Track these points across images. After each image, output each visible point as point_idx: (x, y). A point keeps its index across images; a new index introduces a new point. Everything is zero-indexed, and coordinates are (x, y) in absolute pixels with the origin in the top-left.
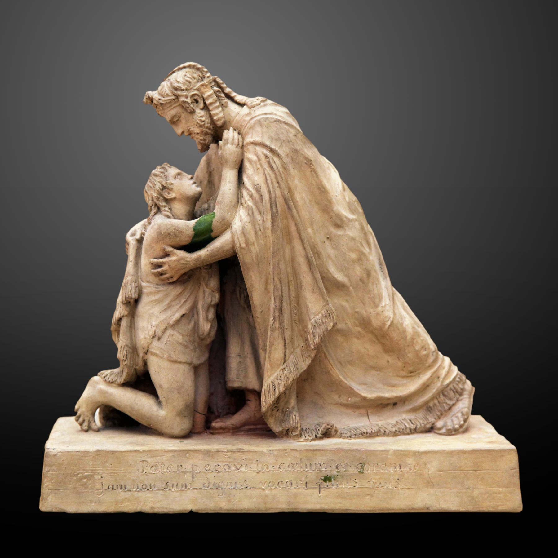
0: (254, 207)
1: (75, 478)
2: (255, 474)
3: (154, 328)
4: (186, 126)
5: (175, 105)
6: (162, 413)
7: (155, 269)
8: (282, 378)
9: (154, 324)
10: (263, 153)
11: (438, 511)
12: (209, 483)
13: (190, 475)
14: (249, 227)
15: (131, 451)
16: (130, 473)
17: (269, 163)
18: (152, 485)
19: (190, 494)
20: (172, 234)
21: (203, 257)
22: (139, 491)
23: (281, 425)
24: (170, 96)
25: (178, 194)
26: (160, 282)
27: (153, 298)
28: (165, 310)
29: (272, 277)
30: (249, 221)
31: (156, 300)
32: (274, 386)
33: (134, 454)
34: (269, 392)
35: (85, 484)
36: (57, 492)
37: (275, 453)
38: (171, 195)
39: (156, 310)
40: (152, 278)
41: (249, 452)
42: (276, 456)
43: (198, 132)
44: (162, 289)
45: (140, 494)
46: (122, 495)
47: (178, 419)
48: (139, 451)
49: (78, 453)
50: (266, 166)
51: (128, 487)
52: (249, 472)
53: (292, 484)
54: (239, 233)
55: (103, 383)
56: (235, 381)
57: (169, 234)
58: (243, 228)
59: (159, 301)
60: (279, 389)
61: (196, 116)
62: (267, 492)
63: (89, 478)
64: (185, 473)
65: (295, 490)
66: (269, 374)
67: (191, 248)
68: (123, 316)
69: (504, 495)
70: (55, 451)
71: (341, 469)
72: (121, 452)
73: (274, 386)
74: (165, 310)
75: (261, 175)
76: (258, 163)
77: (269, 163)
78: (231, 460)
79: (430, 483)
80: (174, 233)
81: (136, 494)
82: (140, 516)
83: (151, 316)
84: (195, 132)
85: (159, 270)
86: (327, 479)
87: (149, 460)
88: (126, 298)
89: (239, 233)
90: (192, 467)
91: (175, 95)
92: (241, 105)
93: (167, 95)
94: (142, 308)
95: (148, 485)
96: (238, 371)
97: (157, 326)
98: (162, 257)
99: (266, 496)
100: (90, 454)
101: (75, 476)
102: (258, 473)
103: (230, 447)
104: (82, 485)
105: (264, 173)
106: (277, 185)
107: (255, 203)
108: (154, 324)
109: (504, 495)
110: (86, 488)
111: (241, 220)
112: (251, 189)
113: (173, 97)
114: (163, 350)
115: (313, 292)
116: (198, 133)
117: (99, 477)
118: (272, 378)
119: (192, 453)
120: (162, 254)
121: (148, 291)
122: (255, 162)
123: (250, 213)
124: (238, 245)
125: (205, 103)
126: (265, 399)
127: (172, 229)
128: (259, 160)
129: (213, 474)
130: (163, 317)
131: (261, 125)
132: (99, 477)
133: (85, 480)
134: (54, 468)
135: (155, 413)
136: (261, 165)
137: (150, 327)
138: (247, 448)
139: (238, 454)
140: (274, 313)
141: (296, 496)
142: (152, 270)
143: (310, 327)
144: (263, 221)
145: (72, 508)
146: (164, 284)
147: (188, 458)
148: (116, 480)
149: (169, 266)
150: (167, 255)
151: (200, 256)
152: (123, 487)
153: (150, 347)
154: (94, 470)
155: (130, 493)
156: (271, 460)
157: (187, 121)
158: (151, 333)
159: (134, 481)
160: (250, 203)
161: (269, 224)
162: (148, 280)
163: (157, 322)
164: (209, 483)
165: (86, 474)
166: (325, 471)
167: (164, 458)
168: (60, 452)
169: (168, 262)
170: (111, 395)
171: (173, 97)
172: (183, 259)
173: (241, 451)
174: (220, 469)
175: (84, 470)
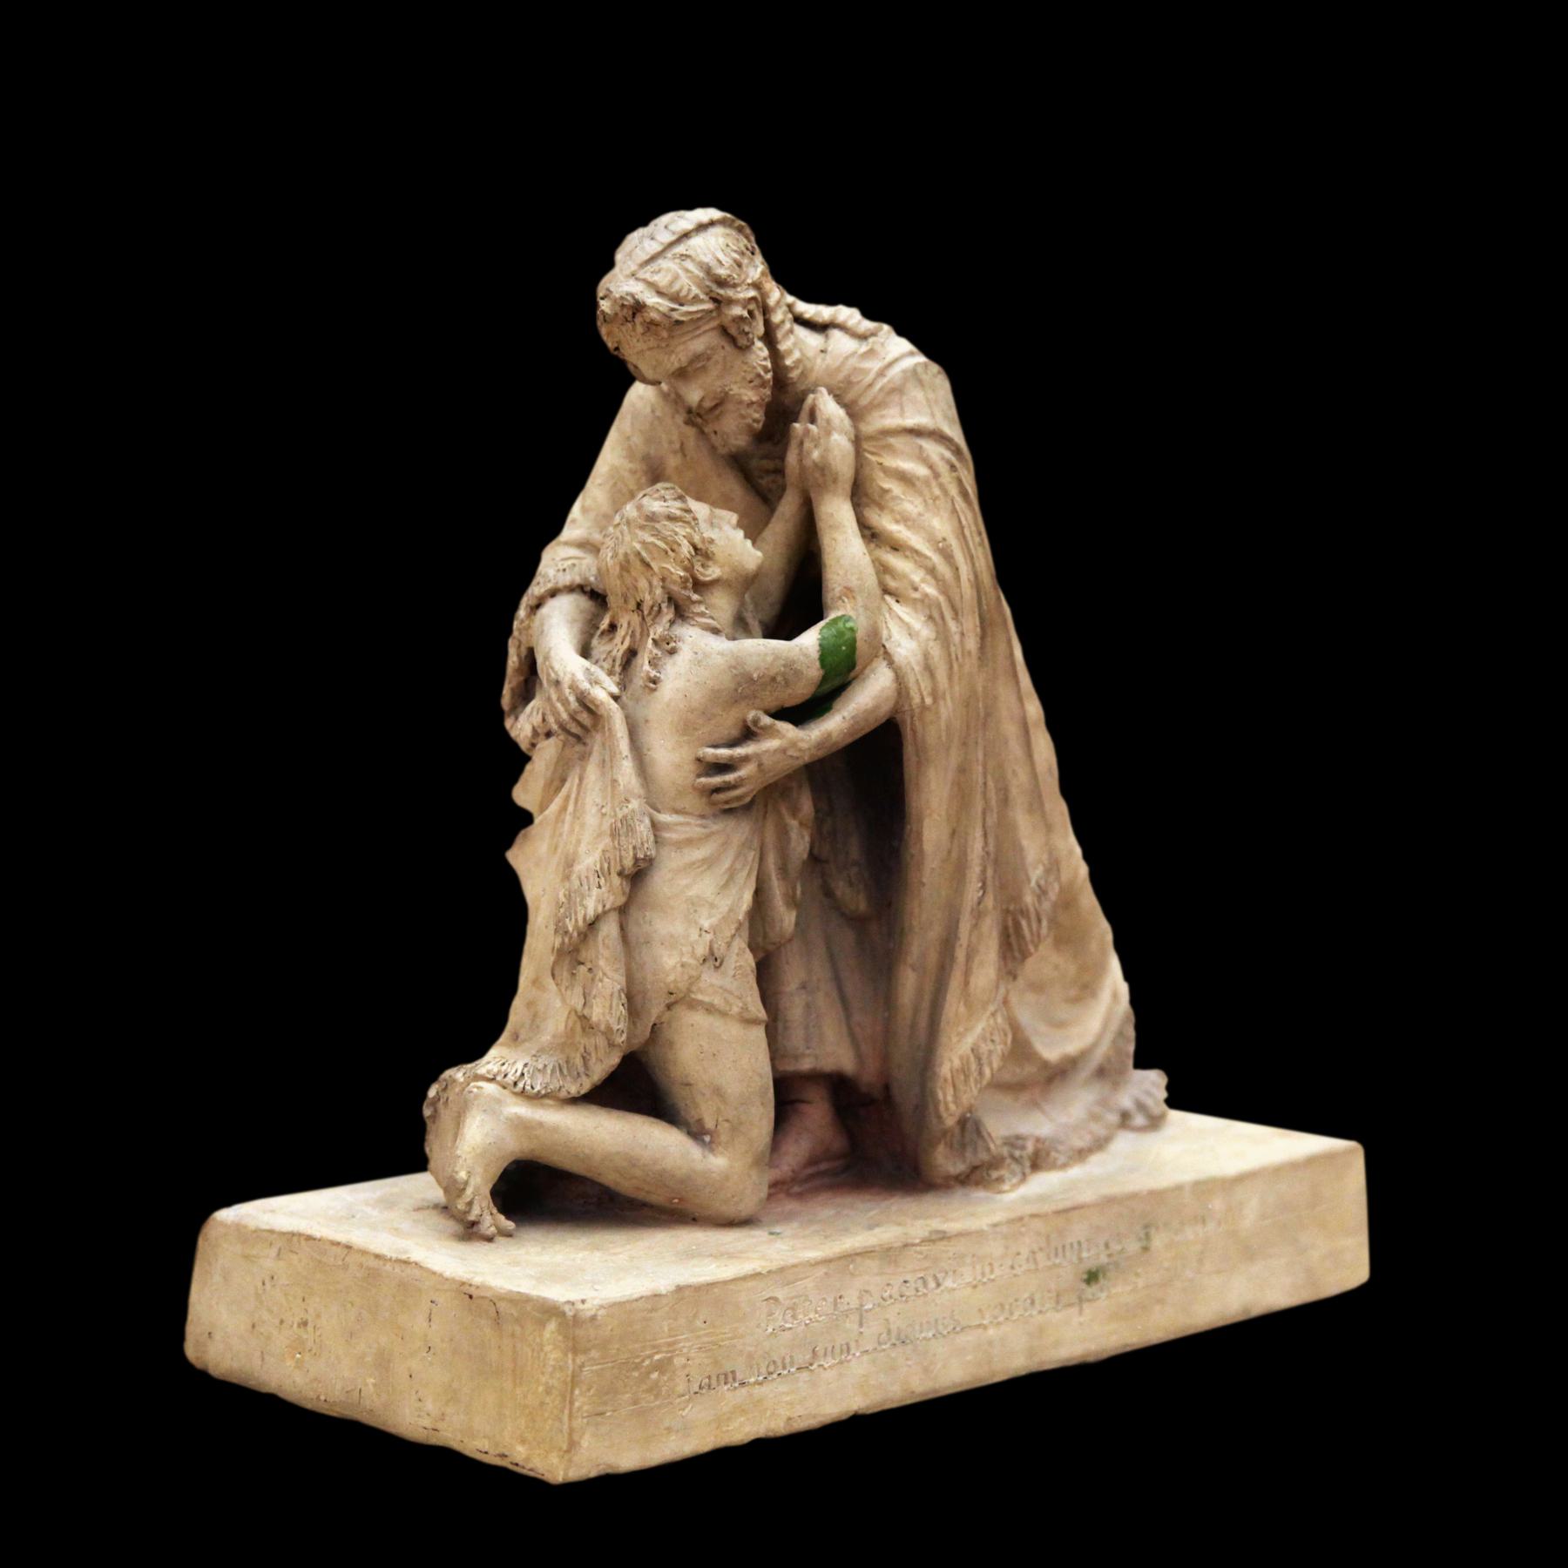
0: (942, 599)
1: (636, 1374)
2: (969, 1290)
3: (708, 937)
4: (718, 383)
5: (707, 327)
6: (718, 1162)
7: (707, 775)
8: (996, 1038)
9: (706, 924)
10: (943, 458)
11: (235, 1381)
12: (889, 1332)
13: (855, 1317)
14: (936, 652)
15: (744, 1278)
16: (742, 1336)
18: (788, 1360)
19: (858, 1367)
20: (779, 679)
21: (834, 735)
22: (760, 1384)
23: (962, 1155)
24: (702, 301)
25: (727, 569)
26: (708, 811)
27: (698, 854)
28: (726, 885)
29: (981, 781)
30: (933, 635)
31: (704, 860)
32: (978, 1059)
33: (751, 1284)
34: (967, 1077)
35: (656, 1383)
36: (599, 1419)
37: (1004, 1229)
38: (709, 572)
39: (706, 886)
40: (693, 802)
41: (960, 1235)
42: (1005, 1237)
43: (754, 399)
44: (715, 828)
45: (765, 1389)
46: (730, 1397)
47: (754, 1174)
48: (759, 1274)
49: (640, 1304)
51: (739, 1376)
52: (959, 1288)
53: (1033, 1302)
54: (917, 668)
55: (513, 1099)
56: (803, 1055)
57: (773, 679)
58: (926, 656)
59: (709, 863)
60: (990, 1064)
61: (753, 357)
62: (991, 1332)
63: (661, 1367)
64: (846, 1314)
65: (1040, 1318)
66: (961, 1029)
67: (801, 714)
68: (605, 913)
69: (1337, 1258)
70: (586, 1306)
71: (1116, 1247)
72: (725, 1283)
73: (978, 1059)
74: (726, 885)
75: (946, 515)
76: (934, 484)
78: (926, 1264)
79: (1249, 1253)
80: (783, 674)
81: (757, 1390)
82: (762, 1448)
83: (695, 903)
84: (745, 398)
85: (717, 780)
86: (1092, 1277)
87: (780, 1294)
88: (636, 860)
89: (917, 668)
90: (860, 1298)
91: (714, 300)
92: (820, 328)
93: (696, 300)
94: (662, 883)
95: (779, 1364)
96: (807, 1028)
97: (715, 930)
98: (732, 744)
99: (990, 1343)
100: (664, 1301)
101: (637, 1367)
102: (975, 1287)
103: (886, 1234)
104: (649, 1390)
105: (954, 511)
107: (944, 590)
108: (706, 924)
109: (1337, 1258)
110: (657, 1397)
111: (912, 634)
112: (929, 553)
113: (709, 306)
114: (731, 993)
115: (1030, 811)
116: (753, 403)
117: (683, 1360)
118: (969, 1040)
119: (859, 1259)
120: (735, 733)
121: (683, 836)
122: (927, 483)
123: (936, 615)
124: (916, 700)
125: (767, 323)
126: (955, 1096)
127: (778, 667)
128: (937, 475)
129: (898, 1307)
130: (724, 904)
132: (683, 1360)
133: (655, 1376)
134: (594, 1354)
135: (699, 1167)
136: (941, 486)
137: (694, 935)
138: (952, 1227)
139: (941, 1246)
140: (984, 871)
141: (1041, 1330)
142: (703, 780)
143: (1029, 899)
144: (962, 634)
145: (629, 1459)
146: (715, 816)
147: (852, 1275)
148: (716, 1362)
149: (760, 765)
150: (748, 733)
151: (829, 735)
152: (728, 1377)
153: (694, 988)
154: (674, 1343)
155: (744, 1391)
156: (995, 1248)
157: (726, 369)
158: (701, 950)
159: (750, 1356)
160: (930, 590)
161: (972, 644)
162: (679, 805)
163: (714, 920)
164: (889, 1332)
165: (657, 1357)
166: (1094, 1257)
167: (809, 1283)
168: (602, 1307)
169: (757, 755)
170: (555, 1129)
171: (709, 306)
172: (794, 744)
173: (943, 1237)
174: (910, 1292)
175: (654, 1347)
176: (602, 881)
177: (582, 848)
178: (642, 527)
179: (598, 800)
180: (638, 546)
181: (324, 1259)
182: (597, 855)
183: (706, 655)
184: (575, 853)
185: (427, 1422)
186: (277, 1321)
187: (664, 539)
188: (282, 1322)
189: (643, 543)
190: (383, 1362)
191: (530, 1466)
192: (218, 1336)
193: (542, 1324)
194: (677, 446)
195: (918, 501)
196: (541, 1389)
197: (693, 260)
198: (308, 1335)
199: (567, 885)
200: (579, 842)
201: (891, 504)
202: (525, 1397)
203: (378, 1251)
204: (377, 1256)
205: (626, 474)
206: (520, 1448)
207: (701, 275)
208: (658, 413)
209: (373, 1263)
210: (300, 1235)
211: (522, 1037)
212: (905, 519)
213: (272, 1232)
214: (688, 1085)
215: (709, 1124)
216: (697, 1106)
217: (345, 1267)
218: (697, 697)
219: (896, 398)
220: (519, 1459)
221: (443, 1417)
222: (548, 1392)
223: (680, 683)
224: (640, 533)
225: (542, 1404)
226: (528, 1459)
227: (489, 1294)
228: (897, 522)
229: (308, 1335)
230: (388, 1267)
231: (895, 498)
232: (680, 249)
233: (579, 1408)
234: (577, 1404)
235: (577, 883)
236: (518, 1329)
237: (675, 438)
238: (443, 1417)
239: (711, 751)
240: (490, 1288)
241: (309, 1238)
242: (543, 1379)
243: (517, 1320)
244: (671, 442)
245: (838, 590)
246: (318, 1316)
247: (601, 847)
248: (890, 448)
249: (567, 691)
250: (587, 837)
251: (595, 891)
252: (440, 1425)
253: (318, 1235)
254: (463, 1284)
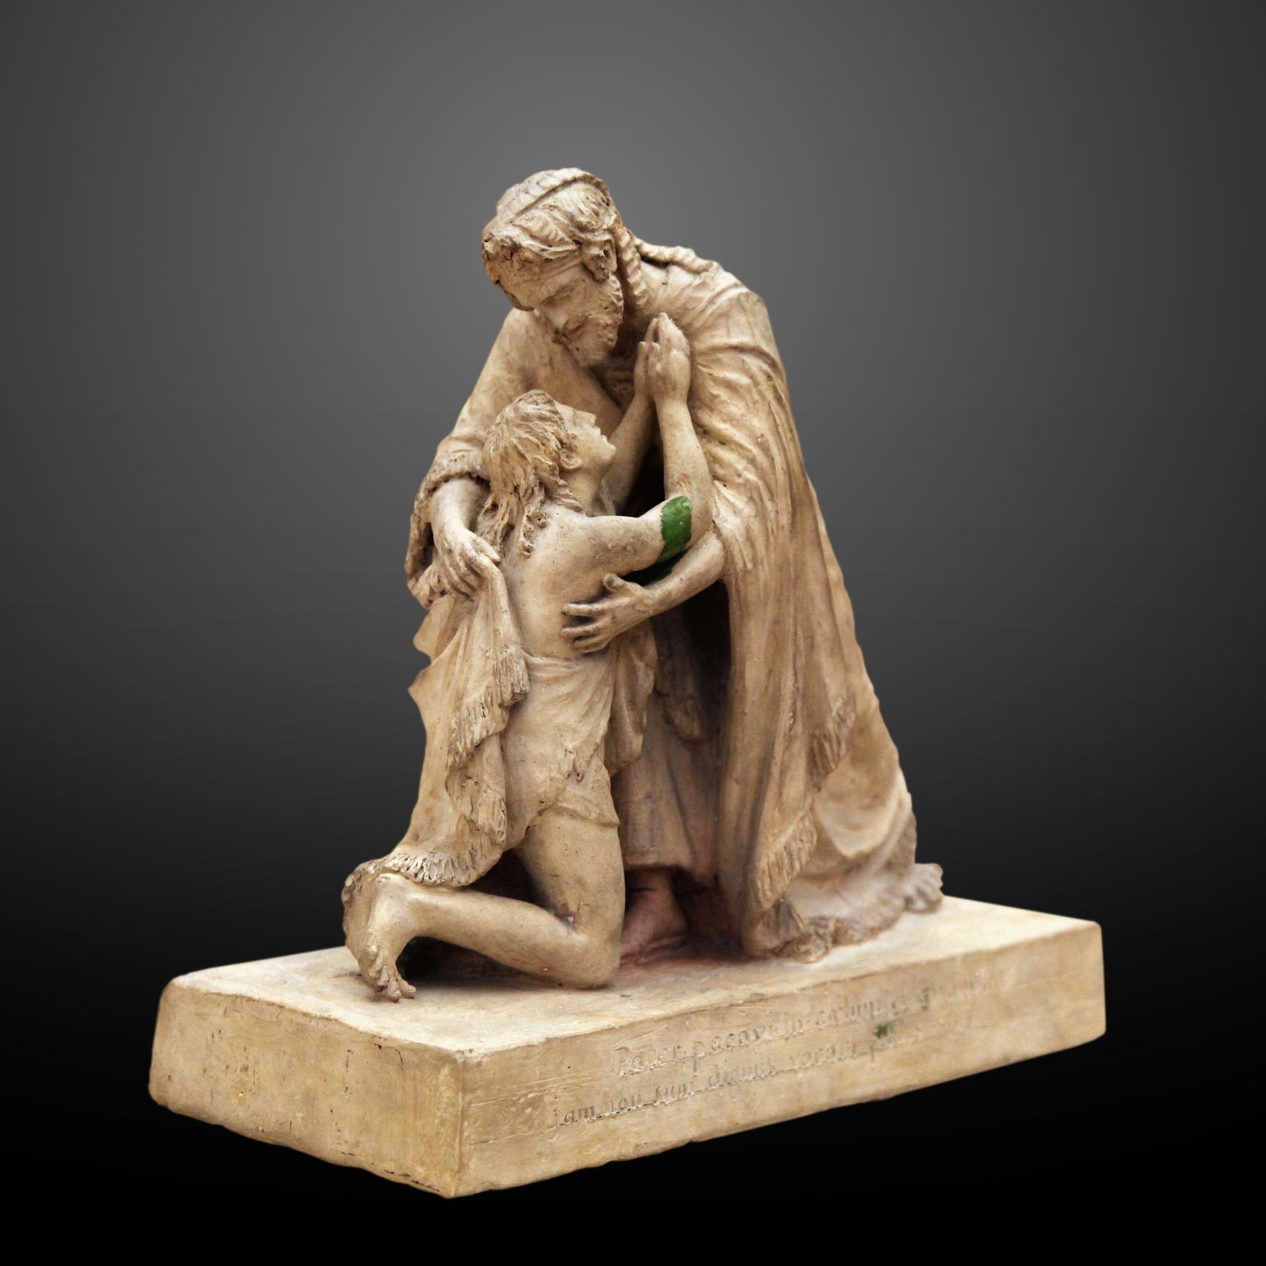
0: (760, 483)
1: (513, 1109)
2: (783, 1041)
3: (572, 757)
4: (580, 309)
5: (571, 264)
6: (580, 938)
7: (571, 625)
8: (804, 838)
9: (570, 746)
10: (761, 370)
12: (718, 1075)
13: (690, 1064)
14: (756, 526)
15: (601, 1032)
16: (599, 1079)
18: (636, 1098)
19: (693, 1104)
20: (629, 548)
21: (674, 594)
22: (614, 1117)
23: (777, 933)
24: (567, 243)
25: (587, 459)
26: (572, 654)
27: (564, 689)
28: (586, 715)
29: (792, 630)
30: (753, 513)
31: (568, 695)
32: (790, 855)
33: (606, 1037)
34: (781, 869)
35: (530, 1117)
36: (484, 1146)
37: (811, 992)
38: (573, 461)
39: (570, 716)
40: (559, 648)
41: (775, 997)
42: (812, 999)
43: (609, 322)
44: (577, 668)
45: (617, 1122)
46: (589, 1128)
47: (609, 948)
48: (613, 1029)
49: (517, 1053)
51: (597, 1111)
52: (774, 1040)
53: (834, 1052)
54: (740, 540)
55: (415, 887)
56: (648, 852)
57: (624, 548)
58: (748, 530)
59: (572, 697)
60: (800, 859)
61: (608, 288)
62: (800, 1075)
63: (534, 1104)
64: (683, 1061)
65: (840, 1064)
66: (776, 831)
67: (647, 576)
68: (488, 737)
69: (1079, 1016)
70: (473, 1054)
71: (901, 1007)
72: (586, 1036)
73: (790, 855)
74: (586, 715)
75: (763, 416)
76: (754, 390)
78: (748, 1021)
80: (633, 545)
81: (611, 1122)
82: (615, 1169)
83: (561, 729)
84: (602, 321)
85: (579, 630)
86: (882, 1031)
87: (630, 1045)
88: (514, 694)
89: (740, 540)
90: (695, 1048)
91: (577, 242)
92: (662, 264)
93: (562, 242)
94: (534, 713)
95: (629, 1101)
96: (651, 830)
97: (577, 751)
98: (591, 601)
99: (800, 1084)
100: (536, 1051)
101: (514, 1104)
102: (787, 1039)
103: (716, 996)
104: (524, 1123)
105: (770, 412)
107: (763, 477)
108: (570, 746)
109: (1079, 1016)
110: (530, 1128)
111: (736, 512)
112: (750, 446)
113: (572, 247)
114: (590, 802)
115: (832, 655)
116: (608, 325)
117: (552, 1098)
118: (783, 840)
119: (693, 1017)
120: (594, 591)
121: (551, 675)
122: (748, 390)
123: (756, 497)
124: (740, 565)
125: (619, 261)
126: (771, 885)
127: (628, 539)
128: (756, 384)
129: (725, 1055)
130: (585, 730)
132: (552, 1098)
133: (529, 1111)
134: (480, 1093)
135: (565, 942)
136: (760, 393)
137: (561, 755)
138: (769, 990)
139: (760, 1006)
140: (794, 704)
141: (841, 1074)
142: (567, 630)
143: (831, 726)
144: (777, 512)
145: (508, 1178)
146: (577, 659)
147: (688, 1029)
148: (578, 1100)
149: (614, 618)
150: (604, 592)
151: (670, 593)
152: (588, 1112)
153: (560, 798)
154: (544, 1084)
155: (600, 1123)
156: (803, 1008)
157: (587, 298)
158: (566, 767)
159: (606, 1095)
160: (751, 476)
161: (785, 520)
162: (548, 650)
163: (577, 743)
164: (718, 1075)
165: (530, 1096)
166: (883, 1015)
167: (653, 1036)
168: (486, 1055)
169: (611, 610)
170: (448, 912)
171: (572, 247)
172: (641, 601)
173: (761, 998)
174: (734, 1043)
175: (528, 1087)
176: (486, 711)
177: (470, 685)
178: (518, 426)
179: (483, 646)
180: (515, 441)
181: (262, 1017)
182: (482, 690)
183: (570, 529)
184: (465, 689)
185: (344, 1148)
186: (224, 1067)
187: (536, 435)
188: (227, 1067)
189: (519, 438)
190: (309, 1100)
191: (428, 1183)
192: (176, 1079)
193: (438, 1069)
194: (547, 360)
195: (741, 405)
196: (437, 1121)
197: (560, 210)
198: (249, 1078)
199: (458, 714)
200: (467, 680)
201: (719, 407)
202: (424, 1128)
203: (305, 1010)
204: (305, 1014)
205: (506, 383)
206: (420, 1169)
207: (566, 222)
208: (531, 334)
209: (301, 1020)
210: (242, 997)
211: (421, 837)
212: (730, 419)
213: (219, 994)
214: (556, 876)
215: (573, 907)
216: (563, 893)
217: (279, 1023)
218: (563, 563)
219: (723, 321)
220: (419, 1178)
221: (357, 1144)
222: (442, 1124)
223: (549, 552)
224: (517, 430)
225: (438, 1133)
226: (426, 1178)
227: (394, 1045)
228: (724, 421)
229: (249, 1078)
230: (313, 1023)
231: (723, 402)
232: (549, 201)
233: (468, 1137)
234: (466, 1134)
235: (466, 713)
236: (418, 1073)
237: (545, 353)
238: (357, 1144)
239: (574, 606)
240: (395, 1040)
241: (250, 1000)
242: (439, 1114)
243: (418, 1066)
244: (541, 357)
245: (676, 476)
246: (257, 1063)
247: (485, 684)
248: (718, 362)
249: (458, 558)
250: (474, 676)
251: (481, 719)
252: (355, 1151)
253: (256, 997)
254: (374, 1036)
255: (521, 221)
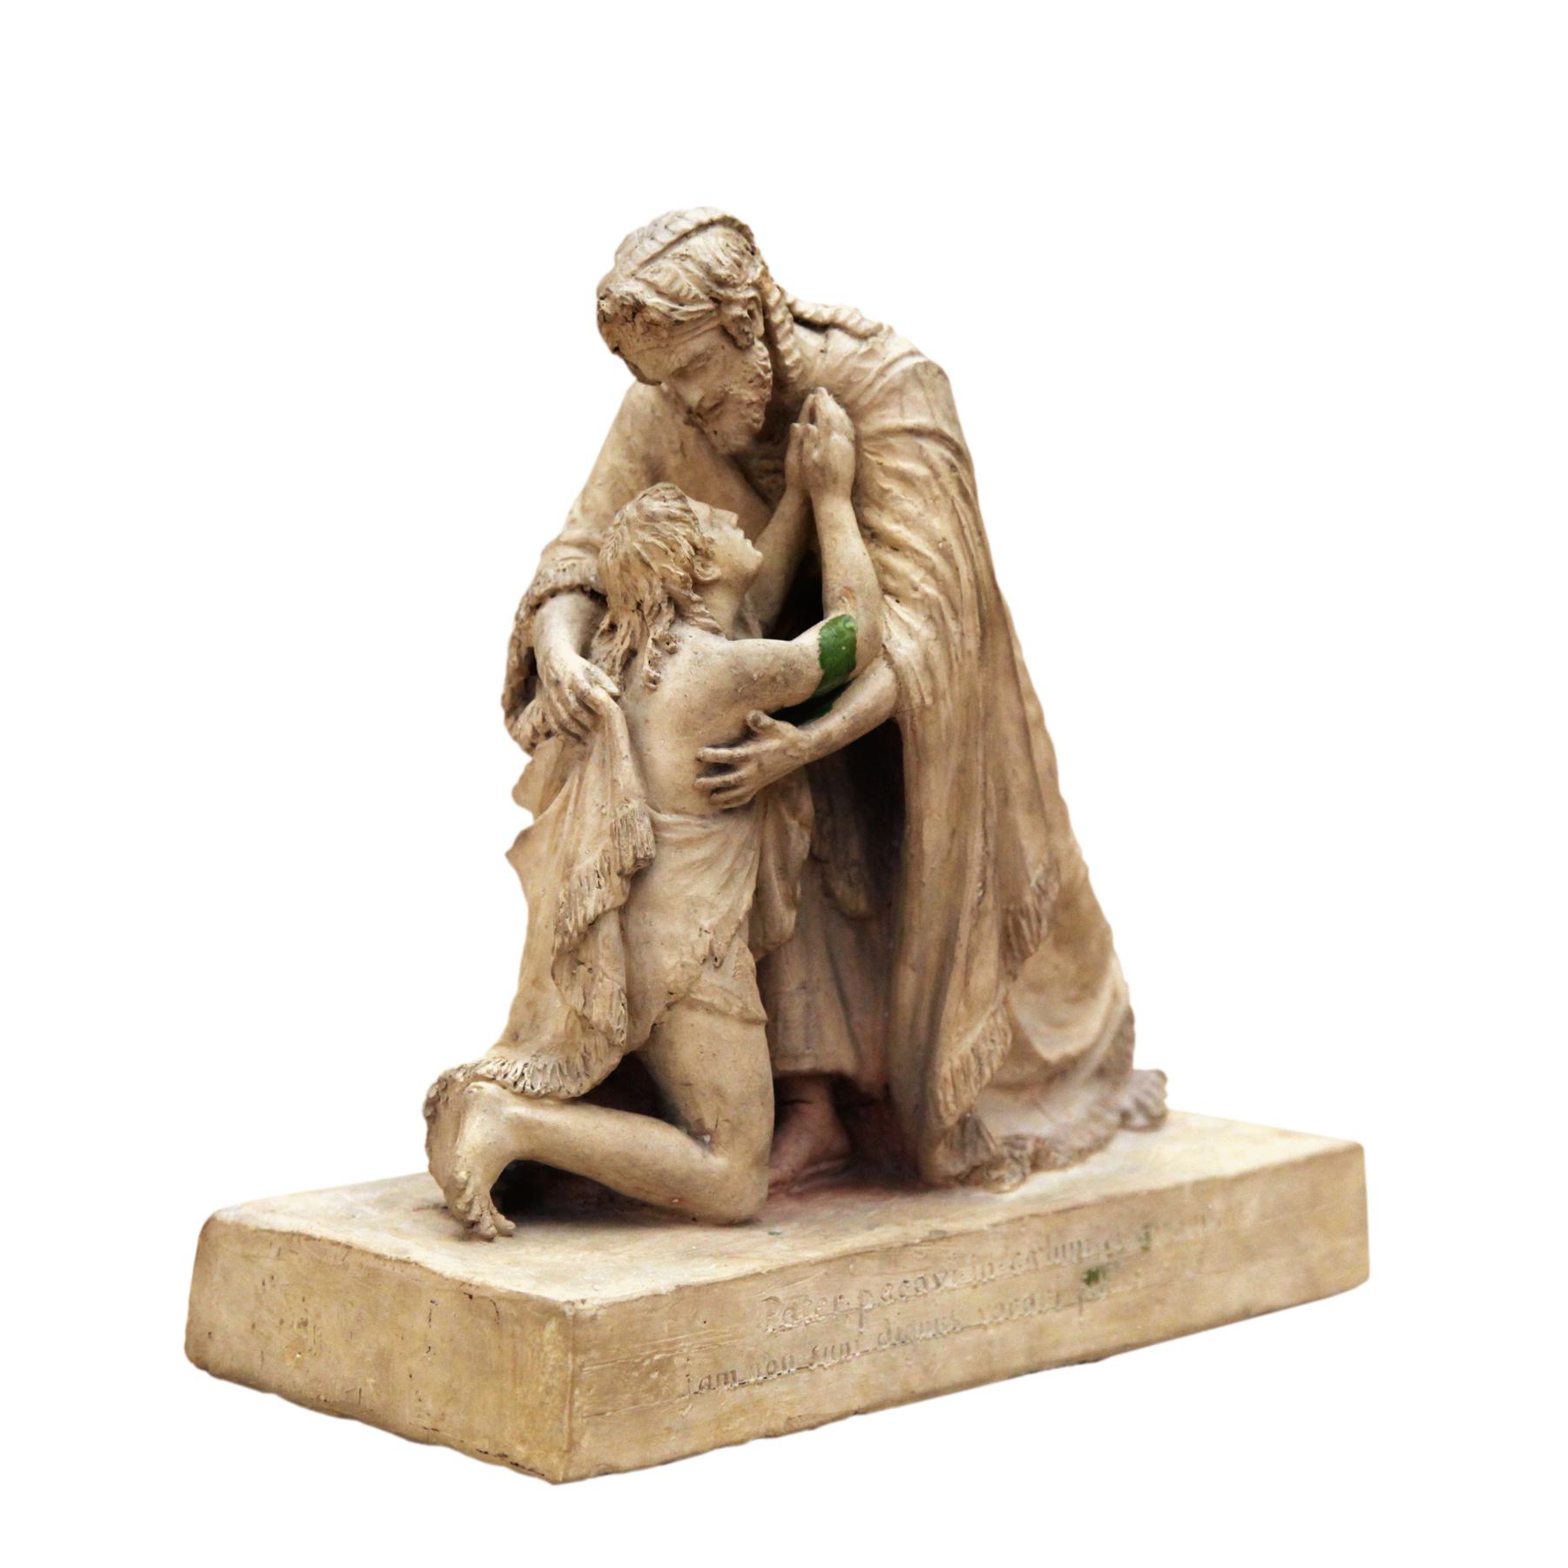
0: (942, 599)
1: (636, 1374)
2: (969, 1290)
3: (708, 937)
4: (718, 383)
5: (707, 327)
6: (718, 1162)
7: (707, 775)
8: (996, 1038)
9: (706, 924)
10: (943, 458)
12: (889, 1332)
13: (855, 1317)
14: (936, 652)
15: (744, 1278)
16: (742, 1336)
17: (960, 481)
18: (788, 1360)
20: (779, 679)
21: (834, 735)
22: (760, 1384)
23: (962, 1155)
24: (702, 301)
25: (727, 569)
26: (708, 811)
27: (698, 854)
28: (726, 885)
29: (981, 781)
30: (933, 635)
31: (704, 860)
32: (978, 1059)
33: (751, 1284)
34: (967, 1077)
35: (656, 1383)
36: (599, 1419)
37: (1004, 1229)
38: (709, 572)
39: (706, 886)
40: (693, 802)
41: (960, 1235)
42: (1005, 1237)
43: (754, 399)
44: (715, 828)
45: (765, 1389)
48: (759, 1274)
49: (640, 1304)
50: (953, 491)
51: (739, 1376)
53: (1033, 1302)
54: (917, 668)
55: (513, 1099)
56: (803, 1055)
57: (773, 679)
58: (926, 656)
59: (709, 863)
60: (990, 1064)
61: (753, 357)
62: (991, 1332)
63: (661, 1367)
64: (846, 1314)
65: (1040, 1318)
66: (961, 1029)
67: (801, 714)
68: (605, 913)
70: (586, 1306)
71: (1116, 1247)
72: (725, 1283)
73: (978, 1059)
74: (726, 885)
75: (946, 515)
76: (934, 484)
77: (960, 481)
78: (926, 1264)
80: (783, 674)
81: (757, 1390)
83: (695, 903)
84: (745, 398)
85: (717, 780)
86: (1092, 1277)
87: (780, 1294)
88: (636, 860)
89: (917, 668)
90: (860, 1298)
91: (714, 300)
93: (696, 300)
94: (662, 883)
95: (779, 1364)
96: (807, 1028)
97: (715, 930)
98: (732, 744)
99: (990, 1343)
100: (664, 1301)
101: (637, 1367)
102: (975, 1287)
103: (886, 1234)
104: (649, 1390)
105: (954, 511)
106: (977, 539)
107: (944, 590)
108: (706, 924)
110: (657, 1397)
111: (912, 634)
112: (929, 553)
113: (709, 306)
114: (731, 993)
115: (1030, 811)
116: (753, 403)
117: (683, 1360)
118: (969, 1040)
119: (859, 1259)
120: (735, 733)
121: (683, 836)
122: (927, 483)
123: (936, 615)
124: (916, 700)
125: (767, 323)
126: (955, 1096)
127: (778, 667)
128: (937, 475)
129: (898, 1307)
130: (724, 904)
131: (921, 383)
132: (683, 1360)
133: (655, 1376)
134: (594, 1354)
135: (699, 1167)
136: (941, 486)
137: (694, 935)
138: (952, 1227)
139: (941, 1246)
140: (984, 871)
141: (1041, 1330)
142: (703, 780)
143: (1029, 899)
144: (962, 634)
146: (715, 816)
147: (852, 1275)
148: (716, 1362)
149: (760, 765)
150: (748, 733)
151: (829, 735)
152: (728, 1377)
153: (694, 988)
154: (674, 1343)
155: (744, 1391)
156: (995, 1248)
157: (726, 369)
158: (701, 950)
159: (750, 1356)
160: (930, 590)
161: (972, 644)
162: (679, 805)
163: (714, 920)
164: (889, 1332)
165: (657, 1357)
166: (1094, 1257)
167: (809, 1283)
168: (602, 1307)
169: (757, 755)
170: (555, 1129)
171: (709, 306)
172: (794, 744)
173: (943, 1237)
174: (910, 1292)
175: (654, 1347)
176: (602, 881)
177: (582, 848)
178: (642, 527)
179: (598, 800)
180: (638, 546)
181: (324, 1259)
182: (597, 855)
183: (706, 655)
184: (575, 853)
186: (277, 1321)
187: (664, 539)
188: (282, 1322)
189: (643, 543)
190: (383, 1362)
192: (218, 1336)
193: (542, 1324)
194: (677, 446)
195: (918, 501)
196: (541, 1389)
197: (693, 260)
198: (308, 1335)
199: (567, 885)
200: (579, 842)
201: (891, 504)
202: (525, 1397)
203: (378, 1251)
204: (377, 1256)
205: (626, 474)
206: (520, 1448)
207: (701, 275)
208: (658, 413)
209: (373, 1263)
210: (300, 1235)
211: (522, 1037)
212: (905, 519)
213: (272, 1232)
214: (688, 1085)
215: (709, 1124)
216: (697, 1106)
217: (345, 1267)
218: (697, 697)
219: (896, 398)
221: (443, 1417)
222: (548, 1392)
223: (680, 683)
224: (640, 533)
225: (542, 1404)
227: (489, 1294)
228: (897, 522)
229: (308, 1335)
230: (388, 1267)
231: (895, 498)
232: (680, 249)
233: (579, 1408)
234: (577, 1404)
235: (577, 883)
236: (518, 1329)
237: (675, 438)
238: (443, 1417)
239: (711, 751)
240: (490, 1288)
241: (309, 1238)
242: (543, 1379)
243: (517, 1320)
244: (671, 442)
245: (838, 590)
246: (318, 1316)
247: (601, 847)
248: (890, 448)
249: (567, 691)
250: (587, 837)
251: (595, 891)
254: (463, 1284)
255: (646, 274)
